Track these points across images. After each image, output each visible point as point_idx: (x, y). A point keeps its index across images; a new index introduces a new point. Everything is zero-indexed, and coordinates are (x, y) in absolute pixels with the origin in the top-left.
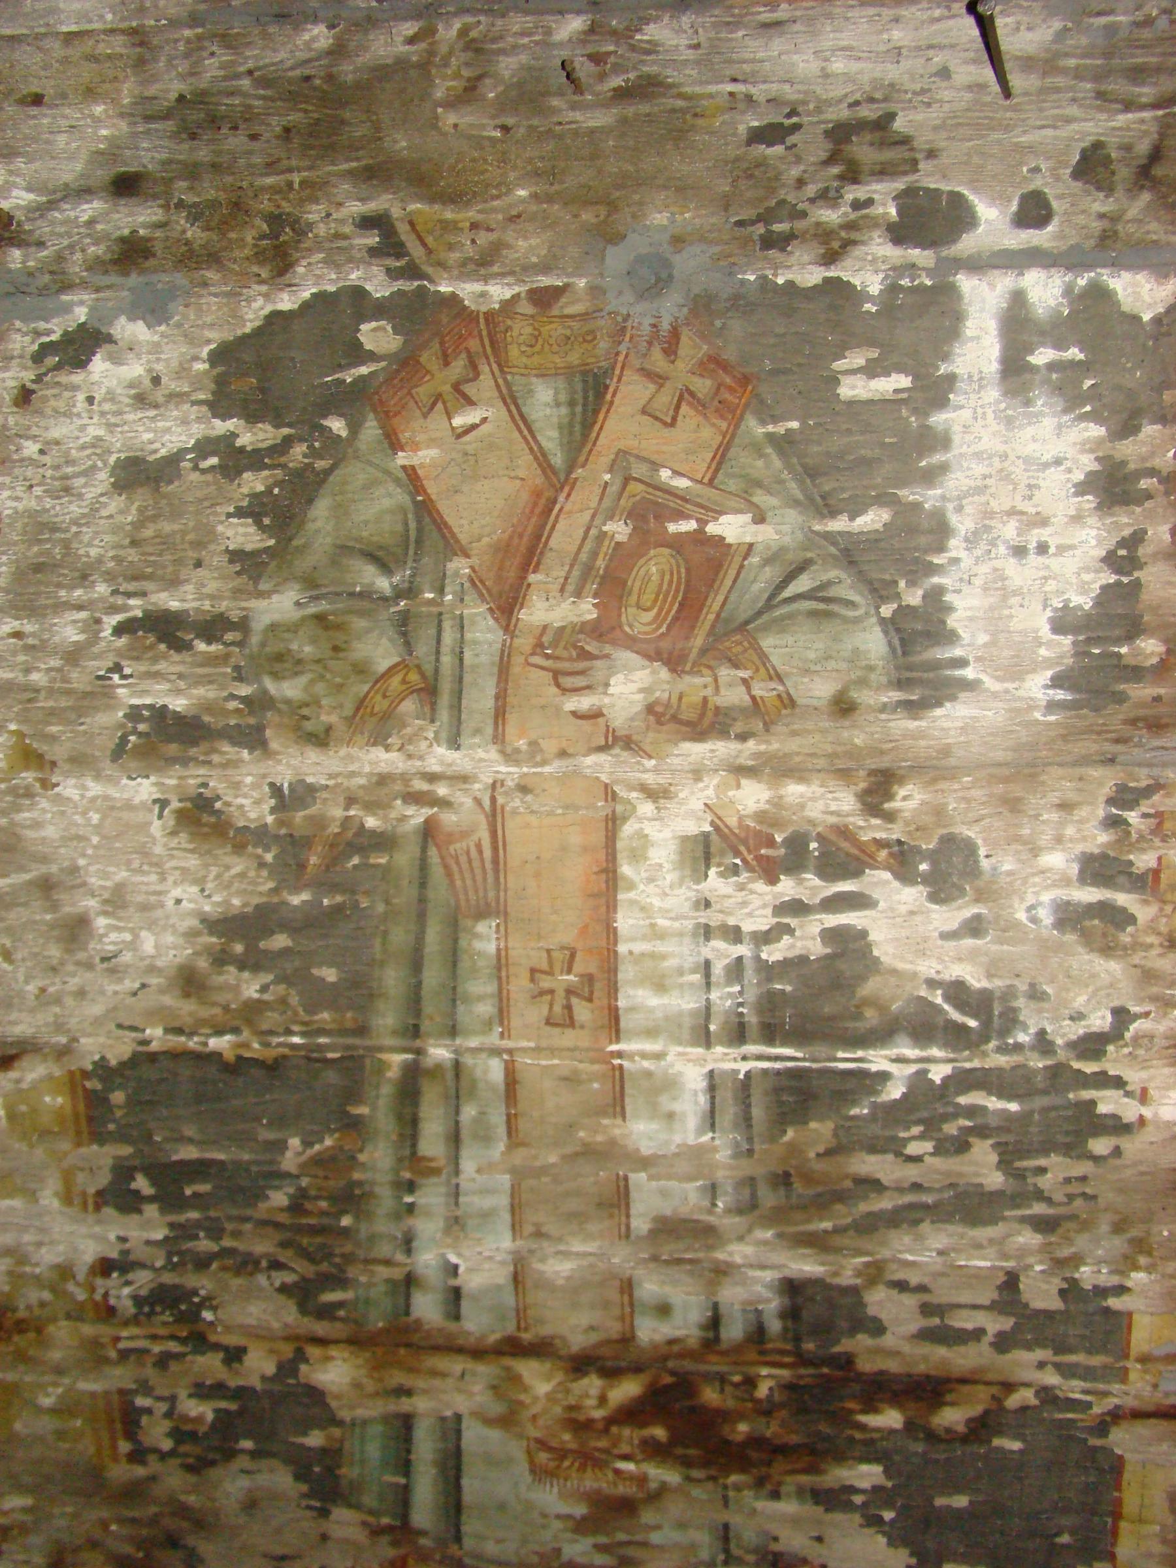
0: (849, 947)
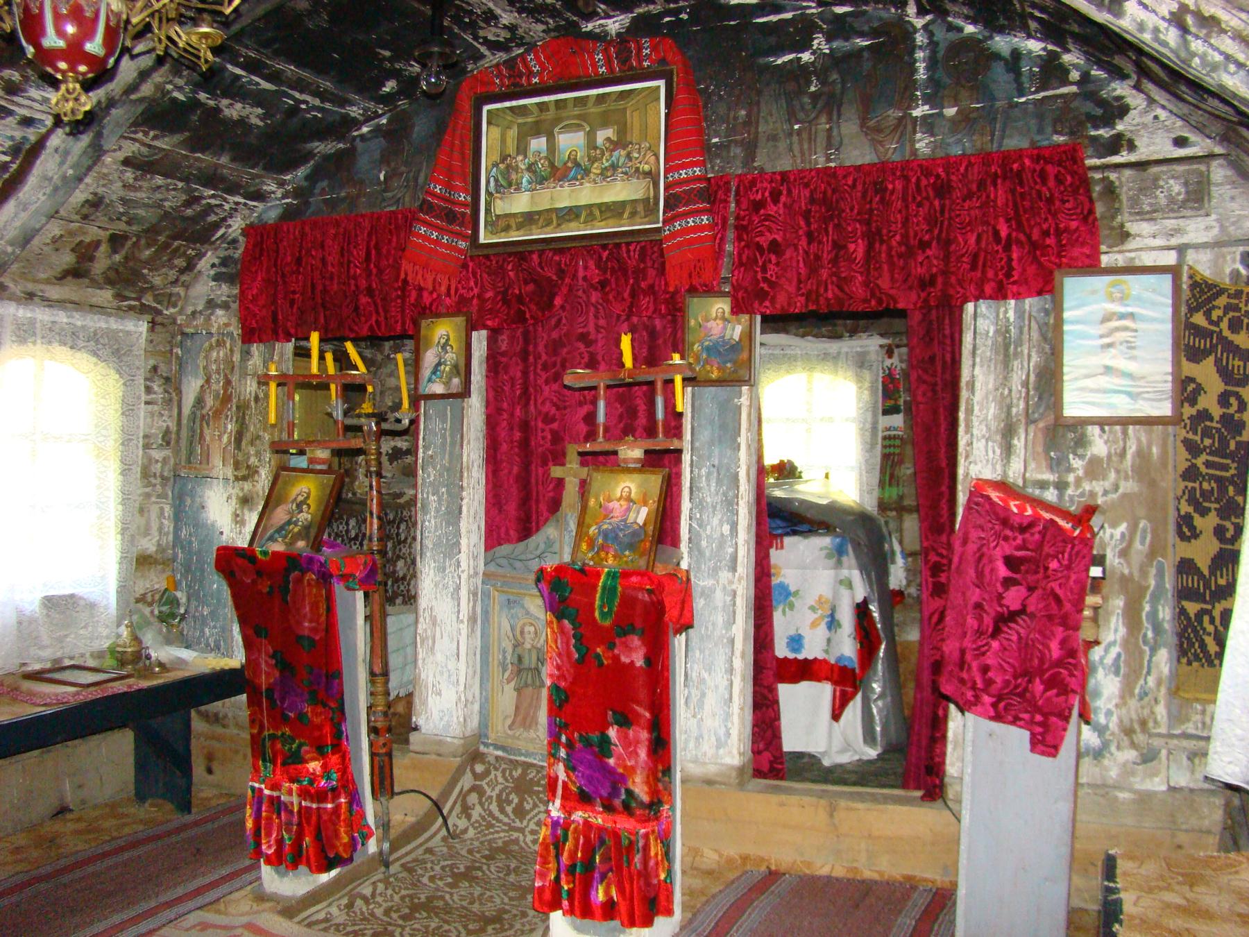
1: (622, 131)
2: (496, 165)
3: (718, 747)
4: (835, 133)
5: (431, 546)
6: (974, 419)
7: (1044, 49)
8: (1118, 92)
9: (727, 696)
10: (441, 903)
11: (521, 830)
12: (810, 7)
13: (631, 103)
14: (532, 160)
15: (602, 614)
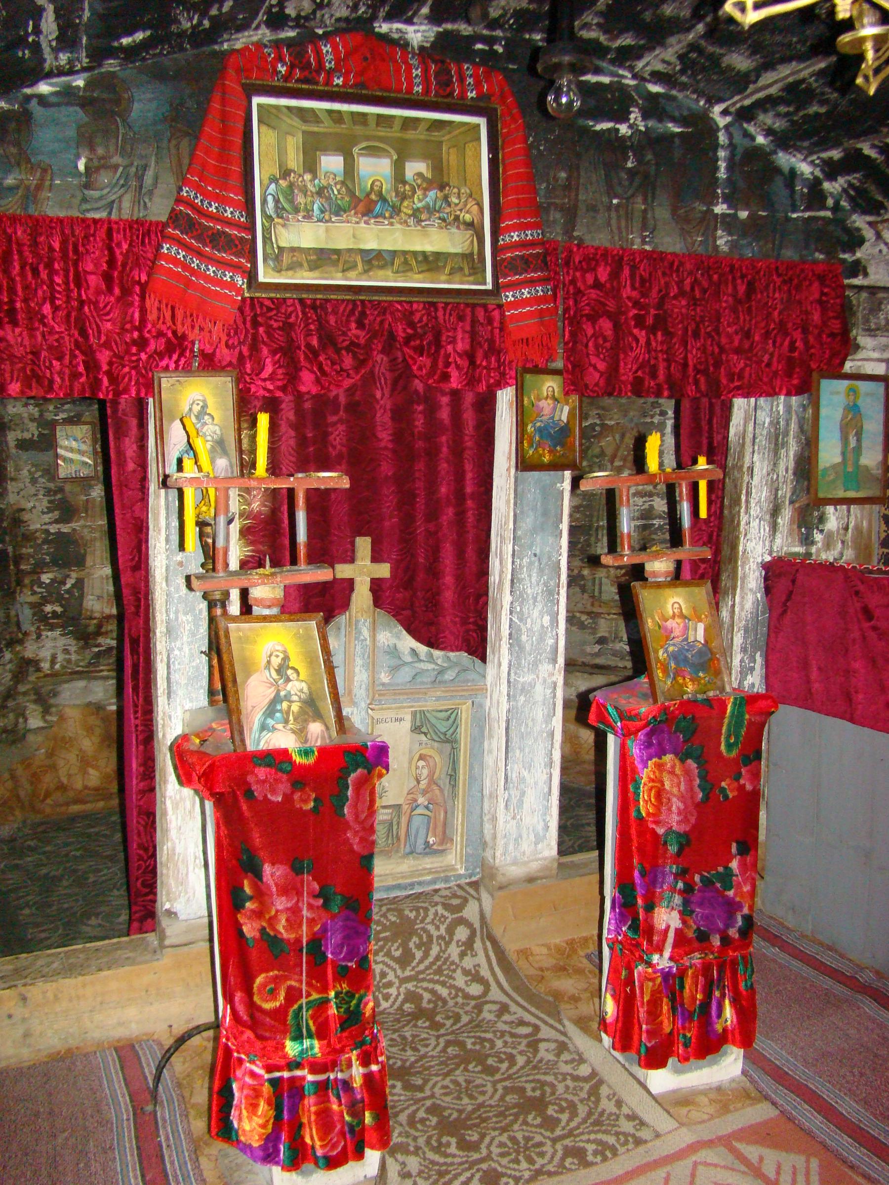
0: (652, 506)
1: (438, 167)
2: (274, 180)
3: (536, 844)
4: (649, 215)
5: (183, 682)
6: (752, 501)
7: (812, 173)
8: (857, 224)
9: (546, 790)
12: (626, 77)
13: (444, 136)
14: (324, 183)
15: (730, 746)
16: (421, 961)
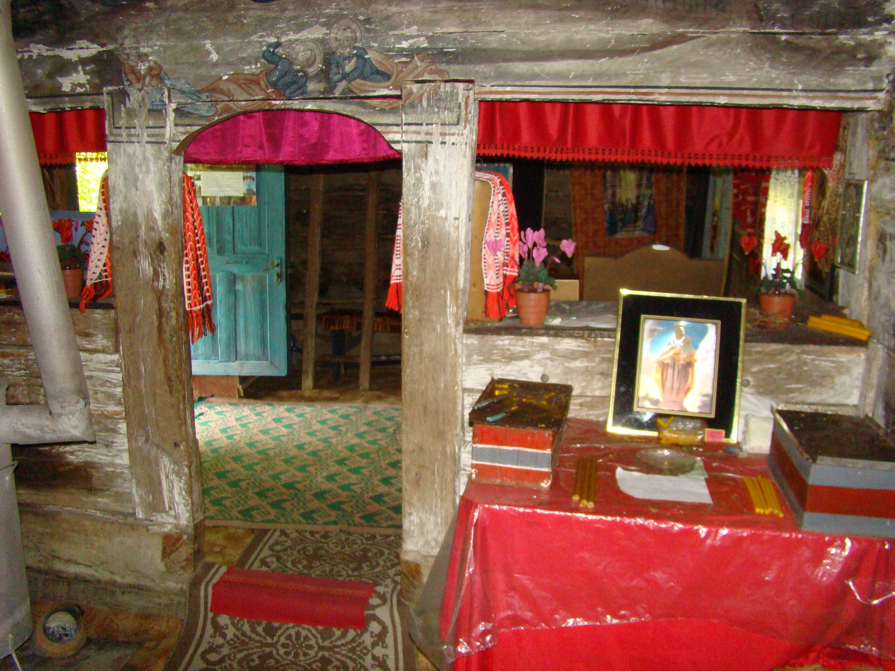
10: (351, 566)
11: (321, 648)
16: (339, 639)
